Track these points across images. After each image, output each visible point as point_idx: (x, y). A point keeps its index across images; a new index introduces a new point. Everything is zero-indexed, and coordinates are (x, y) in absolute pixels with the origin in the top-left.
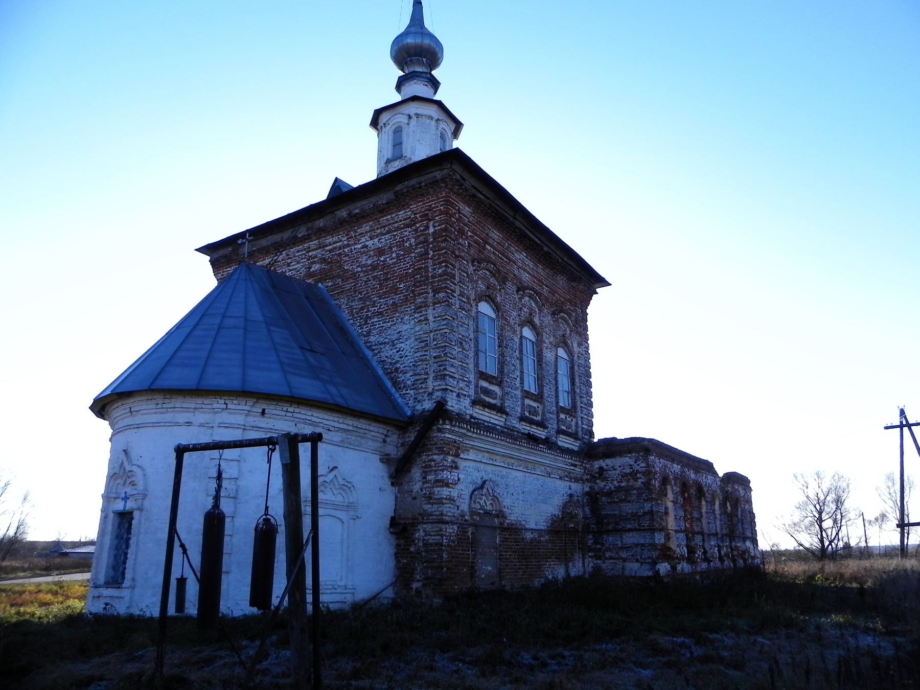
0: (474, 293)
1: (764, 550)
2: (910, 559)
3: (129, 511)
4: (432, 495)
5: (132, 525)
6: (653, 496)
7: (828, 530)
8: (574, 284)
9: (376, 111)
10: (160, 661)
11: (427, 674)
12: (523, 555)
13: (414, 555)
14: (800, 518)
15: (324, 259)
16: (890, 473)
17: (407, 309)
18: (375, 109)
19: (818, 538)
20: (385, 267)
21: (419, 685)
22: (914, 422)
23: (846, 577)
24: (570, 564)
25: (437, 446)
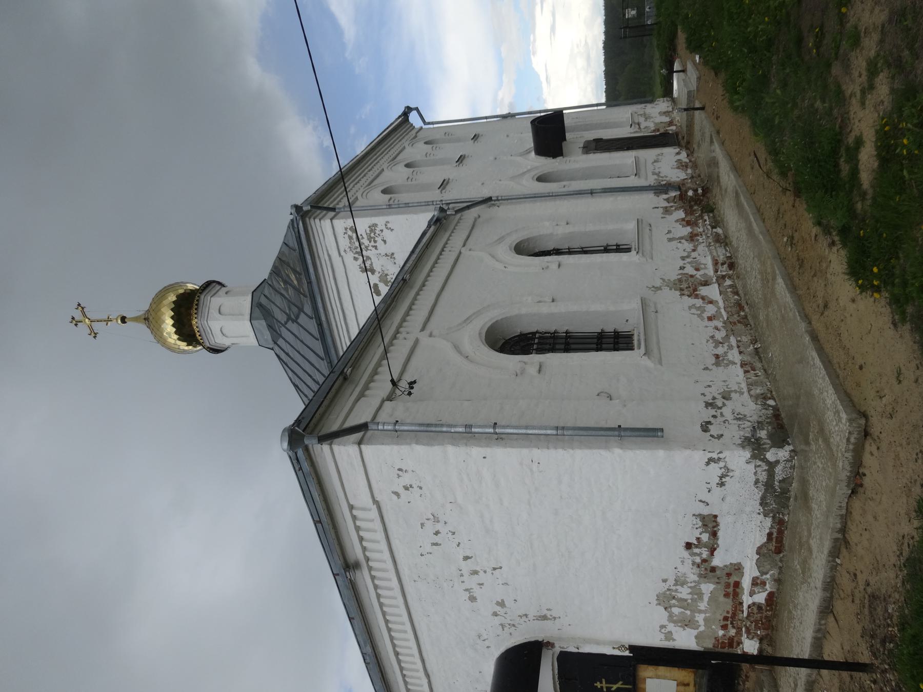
11: (805, 336)
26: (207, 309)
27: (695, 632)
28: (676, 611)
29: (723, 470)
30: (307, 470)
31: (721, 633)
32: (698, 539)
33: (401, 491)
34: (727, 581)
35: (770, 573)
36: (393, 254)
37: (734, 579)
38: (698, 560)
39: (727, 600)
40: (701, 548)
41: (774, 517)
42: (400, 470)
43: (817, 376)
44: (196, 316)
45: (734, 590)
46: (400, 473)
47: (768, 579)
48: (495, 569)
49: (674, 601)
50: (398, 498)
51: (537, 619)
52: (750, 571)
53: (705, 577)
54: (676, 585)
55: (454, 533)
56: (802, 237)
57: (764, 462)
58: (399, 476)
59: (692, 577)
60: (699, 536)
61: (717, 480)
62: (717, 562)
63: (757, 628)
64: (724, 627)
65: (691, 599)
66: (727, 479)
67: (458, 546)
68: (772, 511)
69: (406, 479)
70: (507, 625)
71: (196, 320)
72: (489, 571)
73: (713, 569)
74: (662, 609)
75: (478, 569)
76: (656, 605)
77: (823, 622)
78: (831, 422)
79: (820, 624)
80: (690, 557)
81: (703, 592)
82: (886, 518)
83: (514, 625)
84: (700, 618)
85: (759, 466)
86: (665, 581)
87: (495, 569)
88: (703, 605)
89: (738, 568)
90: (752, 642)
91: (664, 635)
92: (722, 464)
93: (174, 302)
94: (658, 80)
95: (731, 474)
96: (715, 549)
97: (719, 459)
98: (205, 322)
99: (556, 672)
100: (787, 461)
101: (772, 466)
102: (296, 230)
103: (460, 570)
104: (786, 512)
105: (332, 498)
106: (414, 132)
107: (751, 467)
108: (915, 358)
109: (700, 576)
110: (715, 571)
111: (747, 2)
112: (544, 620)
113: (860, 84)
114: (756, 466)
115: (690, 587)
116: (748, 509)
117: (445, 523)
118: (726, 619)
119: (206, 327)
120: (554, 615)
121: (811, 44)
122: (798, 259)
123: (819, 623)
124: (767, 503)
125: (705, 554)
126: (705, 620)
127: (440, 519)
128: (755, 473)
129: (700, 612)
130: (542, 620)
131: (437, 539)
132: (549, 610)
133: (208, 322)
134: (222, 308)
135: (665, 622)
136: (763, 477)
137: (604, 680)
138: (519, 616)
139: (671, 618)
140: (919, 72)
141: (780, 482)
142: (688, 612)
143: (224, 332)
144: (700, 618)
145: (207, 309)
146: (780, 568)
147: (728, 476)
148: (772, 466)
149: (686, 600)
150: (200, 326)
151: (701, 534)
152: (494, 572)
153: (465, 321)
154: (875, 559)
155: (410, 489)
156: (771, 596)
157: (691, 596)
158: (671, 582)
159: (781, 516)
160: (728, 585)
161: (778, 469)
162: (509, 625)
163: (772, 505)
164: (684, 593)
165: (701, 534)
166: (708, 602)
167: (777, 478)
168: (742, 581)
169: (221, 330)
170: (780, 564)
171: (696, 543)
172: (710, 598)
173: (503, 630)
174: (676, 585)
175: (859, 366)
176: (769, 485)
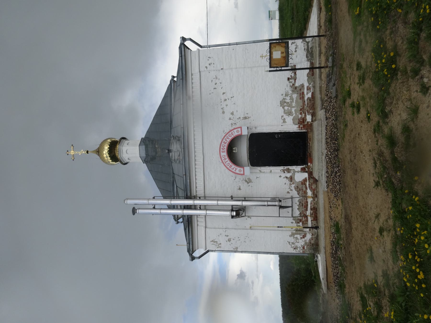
9: (179, 48)
18: (173, 218)
26: (123, 143)
27: (292, 117)
28: (286, 108)
29: (296, 46)
31: (300, 116)
32: (291, 76)
33: (208, 66)
34: (300, 92)
37: (302, 91)
38: (291, 85)
39: (300, 100)
40: (292, 80)
41: (310, 61)
42: (209, 57)
44: (119, 144)
45: (302, 96)
46: (209, 59)
47: (311, 87)
48: (232, 97)
49: (285, 104)
50: (207, 69)
51: (243, 119)
52: (306, 84)
53: (294, 92)
54: (285, 96)
55: (221, 83)
57: (306, 42)
59: (290, 92)
60: (291, 75)
61: (294, 50)
62: (297, 85)
63: (310, 109)
64: (301, 114)
65: (290, 102)
66: (297, 49)
67: (222, 88)
68: (309, 59)
69: (211, 61)
70: (233, 124)
71: (118, 146)
72: (230, 98)
73: (296, 88)
74: (282, 108)
75: (226, 98)
76: (280, 106)
77: (320, 60)
79: (320, 61)
80: (289, 83)
81: (294, 98)
83: (236, 124)
84: (293, 110)
85: (305, 43)
86: (282, 95)
87: (232, 97)
88: (294, 104)
89: (302, 86)
90: (309, 116)
91: (283, 120)
92: (295, 44)
93: (110, 143)
95: (297, 47)
96: (296, 79)
97: (294, 42)
98: (121, 147)
99: (248, 147)
100: (311, 41)
101: (308, 43)
103: (221, 100)
104: (313, 59)
105: (187, 70)
107: (303, 44)
109: (292, 91)
112: (245, 119)
114: (304, 44)
115: (290, 96)
116: (303, 60)
117: (219, 79)
118: (301, 110)
119: (121, 150)
120: (249, 117)
123: (319, 60)
124: (308, 57)
125: (293, 81)
126: (295, 111)
127: (217, 78)
128: (304, 46)
129: (293, 107)
130: (245, 119)
131: (216, 86)
132: (247, 114)
133: (123, 147)
134: (127, 150)
135: (283, 114)
136: (306, 47)
139: (285, 112)
141: (310, 48)
142: (290, 108)
143: (127, 152)
144: (293, 110)
145: (123, 143)
146: (314, 81)
147: (297, 48)
148: (308, 43)
149: (289, 103)
150: (119, 148)
151: (292, 74)
152: (231, 99)
153: (325, 230)
155: (211, 65)
156: (313, 93)
157: (290, 100)
158: (284, 95)
159: (312, 61)
160: (300, 94)
161: (310, 44)
162: (234, 123)
163: (309, 57)
164: (288, 100)
165: (292, 74)
166: (295, 102)
167: (309, 47)
168: (304, 91)
169: (127, 150)
170: (314, 80)
171: (291, 78)
172: (296, 100)
174: (285, 96)
176: (308, 50)
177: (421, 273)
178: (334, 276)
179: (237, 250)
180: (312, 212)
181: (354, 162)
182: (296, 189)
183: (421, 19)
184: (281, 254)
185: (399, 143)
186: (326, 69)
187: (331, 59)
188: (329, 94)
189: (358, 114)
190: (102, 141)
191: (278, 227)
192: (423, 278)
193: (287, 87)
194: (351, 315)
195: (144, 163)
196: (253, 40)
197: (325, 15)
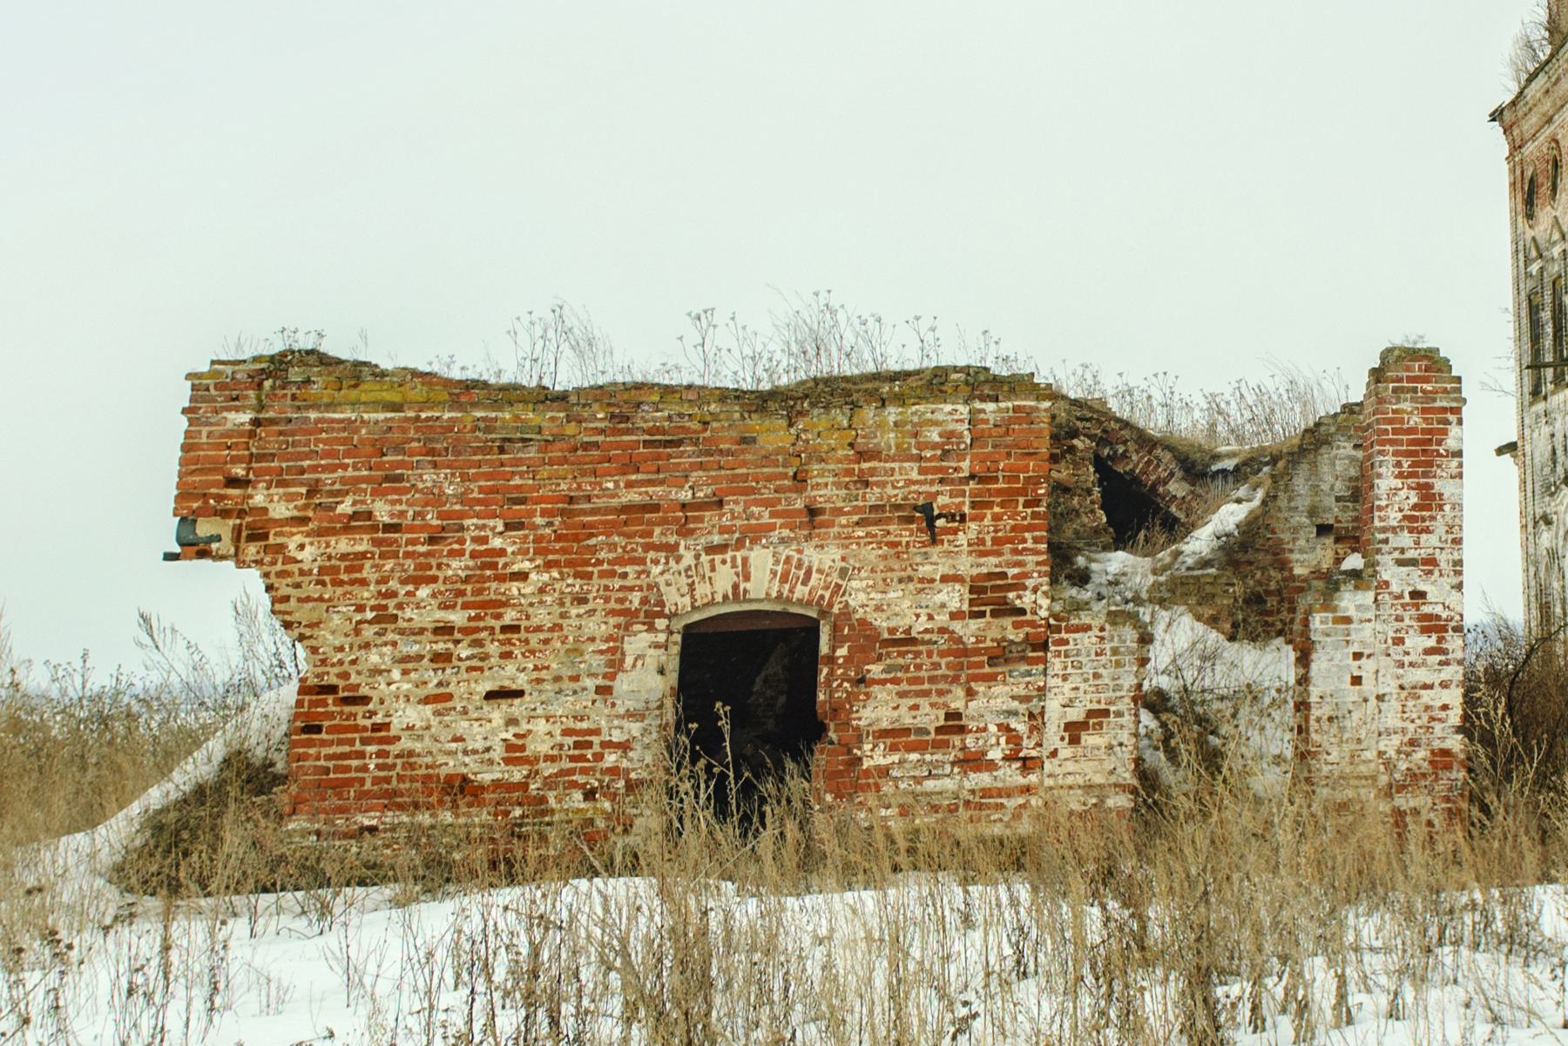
0: (714, 1014)
1: (175, 492)
2: (1263, 449)
3: (1067, 484)
4: (861, 877)
5: (516, 387)
6: (254, 450)
7: (1290, 654)
8: (629, 661)
10: (29, 812)
11: (747, 911)
12: (282, 574)
13: (914, 688)
14: (1021, 358)
15: (628, 1018)
16: (1459, 380)
17: (573, 765)
19: (1540, 1018)
20: (853, 967)
21: (1285, 761)
22: (224, 563)
23: (1520, 631)
24: (1233, 990)
25: (647, 540)
30: (1177, 979)
35: (485, 547)
36: (1496, 116)
43: (1478, 825)
56: (1473, 901)
58: (509, 332)
78: (573, 663)
82: (417, 791)
94: (415, 536)
102: (939, 913)
106: (197, 382)
108: (711, 549)
110: (1404, 644)
111: (608, 1028)
113: (517, 701)
121: (1225, 602)
122: (1071, 700)
129: (1547, 365)
137: (720, 724)
138: (1500, 451)
140: (1559, 649)
154: (172, 977)
173: (1530, 216)
175: (658, 505)
177: (1079, 592)
178: (1055, 438)
179: (1562, 33)
180: (1177, 1011)
181: (1111, 392)
182: (267, 569)
183: (518, 812)
184: (229, 370)
185: (1431, 642)
186: (233, 352)
187: (488, 688)
188: (599, 757)
189: (119, 874)
190: (955, 353)
191: (157, 647)
192: (1520, 631)
193: (1472, 1004)
194: (945, 579)
195: (213, 362)
196: (206, 563)
197: (1216, 543)
